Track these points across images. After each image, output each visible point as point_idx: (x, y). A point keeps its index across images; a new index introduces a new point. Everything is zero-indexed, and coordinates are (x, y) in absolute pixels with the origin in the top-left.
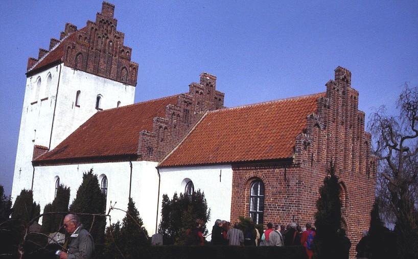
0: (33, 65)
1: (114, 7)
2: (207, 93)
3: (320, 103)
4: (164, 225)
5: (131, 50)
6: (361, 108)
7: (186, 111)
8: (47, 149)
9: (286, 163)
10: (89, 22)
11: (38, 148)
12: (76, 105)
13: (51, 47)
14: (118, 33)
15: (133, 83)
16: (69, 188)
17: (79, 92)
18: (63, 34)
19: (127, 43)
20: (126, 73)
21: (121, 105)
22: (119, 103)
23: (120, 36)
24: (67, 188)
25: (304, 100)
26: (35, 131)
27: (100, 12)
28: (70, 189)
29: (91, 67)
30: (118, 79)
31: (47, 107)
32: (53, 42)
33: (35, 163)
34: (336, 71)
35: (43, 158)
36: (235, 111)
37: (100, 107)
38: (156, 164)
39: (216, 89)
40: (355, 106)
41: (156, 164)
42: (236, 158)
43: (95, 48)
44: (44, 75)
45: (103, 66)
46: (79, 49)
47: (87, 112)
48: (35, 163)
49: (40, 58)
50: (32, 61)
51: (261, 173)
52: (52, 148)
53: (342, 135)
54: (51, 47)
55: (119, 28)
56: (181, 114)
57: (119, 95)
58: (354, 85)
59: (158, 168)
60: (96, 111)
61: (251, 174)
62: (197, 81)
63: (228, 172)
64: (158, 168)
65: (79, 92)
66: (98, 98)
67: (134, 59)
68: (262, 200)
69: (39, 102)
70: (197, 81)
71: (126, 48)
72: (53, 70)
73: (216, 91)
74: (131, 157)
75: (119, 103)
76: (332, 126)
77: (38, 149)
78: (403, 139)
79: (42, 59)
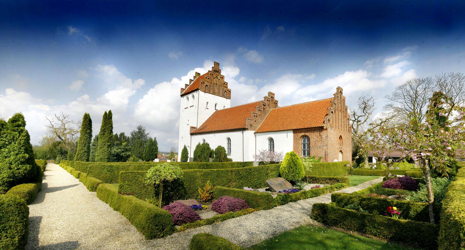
0: (183, 91)
3: (331, 102)
7: (264, 108)
9: (321, 129)
10: (209, 71)
13: (190, 83)
15: (229, 98)
16: (155, 138)
17: (207, 103)
18: (195, 77)
21: (225, 108)
22: (224, 107)
23: (222, 77)
24: (153, 139)
27: (213, 66)
28: (157, 139)
29: (212, 92)
30: (223, 96)
31: (194, 110)
33: (192, 134)
34: (337, 89)
35: (195, 132)
38: (254, 132)
40: (344, 104)
44: (190, 96)
45: (216, 91)
46: (206, 83)
47: (212, 111)
48: (192, 134)
50: (182, 89)
51: (307, 134)
52: (198, 127)
53: (340, 116)
55: (222, 74)
56: (262, 110)
57: (224, 103)
59: (255, 133)
61: (303, 134)
62: (267, 95)
65: (207, 103)
66: (216, 105)
67: (229, 87)
68: (309, 145)
69: (189, 107)
70: (267, 95)
72: (195, 94)
74: (244, 129)
75: (224, 107)
76: (337, 112)
78: (358, 117)
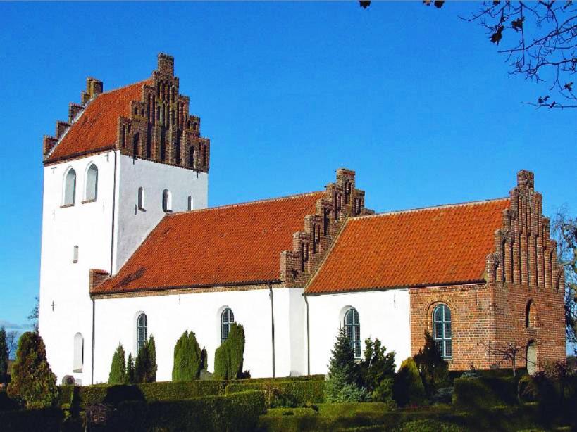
1: (173, 60)
2: (347, 196)
4: (417, 358)
5: (199, 120)
6: (546, 213)
8: (107, 274)
11: (97, 273)
12: (141, 209)
14: (181, 97)
19: (193, 110)
20: (196, 157)
25: (481, 207)
26: (77, 247)
32: (75, 109)
33: (95, 294)
36: (388, 218)
37: (169, 208)
38: (302, 290)
39: (356, 187)
41: (302, 290)
42: (414, 281)
43: (158, 127)
49: (59, 136)
52: (115, 273)
54: (73, 117)
57: (187, 190)
58: (538, 187)
59: (305, 295)
60: (164, 214)
63: (403, 296)
64: (305, 295)
67: (205, 133)
71: (192, 118)
73: (356, 190)
77: (97, 275)
79: (63, 137)
